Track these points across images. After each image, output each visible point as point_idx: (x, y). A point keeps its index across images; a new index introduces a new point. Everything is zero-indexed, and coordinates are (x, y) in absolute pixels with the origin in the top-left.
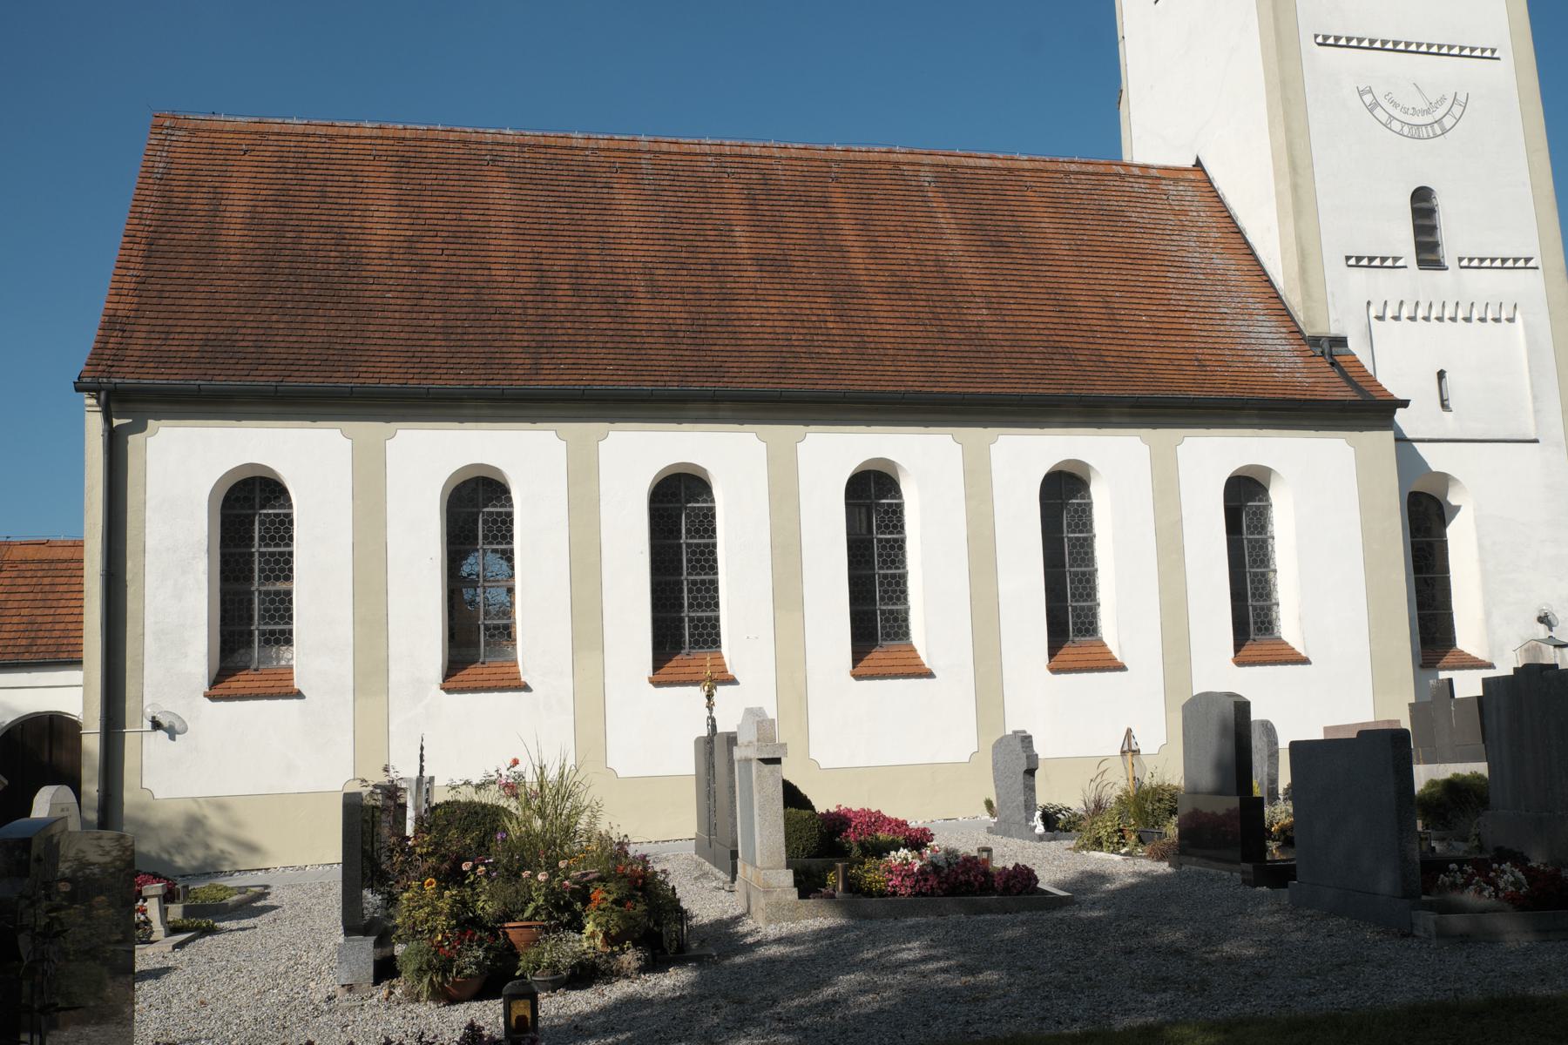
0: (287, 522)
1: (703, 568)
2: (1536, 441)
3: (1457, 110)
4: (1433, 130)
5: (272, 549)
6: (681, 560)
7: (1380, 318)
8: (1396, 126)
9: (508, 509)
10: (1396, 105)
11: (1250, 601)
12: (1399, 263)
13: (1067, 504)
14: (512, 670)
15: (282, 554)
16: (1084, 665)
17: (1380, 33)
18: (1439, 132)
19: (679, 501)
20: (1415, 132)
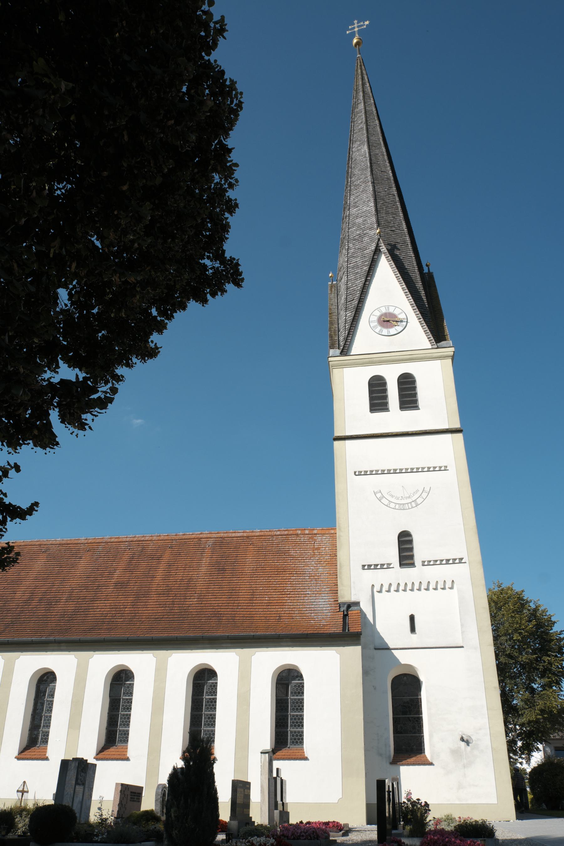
0: (301, 686)
1: (297, 709)
2: (462, 647)
3: (424, 495)
4: (408, 506)
5: (295, 697)
6: (203, 705)
7: (380, 592)
8: (392, 505)
9: (216, 681)
10: (392, 496)
11: (289, 728)
12: (391, 566)
13: (207, 683)
14: (301, 751)
15: (299, 699)
16: (118, 757)
17: (398, 467)
18: (410, 507)
20: (402, 507)
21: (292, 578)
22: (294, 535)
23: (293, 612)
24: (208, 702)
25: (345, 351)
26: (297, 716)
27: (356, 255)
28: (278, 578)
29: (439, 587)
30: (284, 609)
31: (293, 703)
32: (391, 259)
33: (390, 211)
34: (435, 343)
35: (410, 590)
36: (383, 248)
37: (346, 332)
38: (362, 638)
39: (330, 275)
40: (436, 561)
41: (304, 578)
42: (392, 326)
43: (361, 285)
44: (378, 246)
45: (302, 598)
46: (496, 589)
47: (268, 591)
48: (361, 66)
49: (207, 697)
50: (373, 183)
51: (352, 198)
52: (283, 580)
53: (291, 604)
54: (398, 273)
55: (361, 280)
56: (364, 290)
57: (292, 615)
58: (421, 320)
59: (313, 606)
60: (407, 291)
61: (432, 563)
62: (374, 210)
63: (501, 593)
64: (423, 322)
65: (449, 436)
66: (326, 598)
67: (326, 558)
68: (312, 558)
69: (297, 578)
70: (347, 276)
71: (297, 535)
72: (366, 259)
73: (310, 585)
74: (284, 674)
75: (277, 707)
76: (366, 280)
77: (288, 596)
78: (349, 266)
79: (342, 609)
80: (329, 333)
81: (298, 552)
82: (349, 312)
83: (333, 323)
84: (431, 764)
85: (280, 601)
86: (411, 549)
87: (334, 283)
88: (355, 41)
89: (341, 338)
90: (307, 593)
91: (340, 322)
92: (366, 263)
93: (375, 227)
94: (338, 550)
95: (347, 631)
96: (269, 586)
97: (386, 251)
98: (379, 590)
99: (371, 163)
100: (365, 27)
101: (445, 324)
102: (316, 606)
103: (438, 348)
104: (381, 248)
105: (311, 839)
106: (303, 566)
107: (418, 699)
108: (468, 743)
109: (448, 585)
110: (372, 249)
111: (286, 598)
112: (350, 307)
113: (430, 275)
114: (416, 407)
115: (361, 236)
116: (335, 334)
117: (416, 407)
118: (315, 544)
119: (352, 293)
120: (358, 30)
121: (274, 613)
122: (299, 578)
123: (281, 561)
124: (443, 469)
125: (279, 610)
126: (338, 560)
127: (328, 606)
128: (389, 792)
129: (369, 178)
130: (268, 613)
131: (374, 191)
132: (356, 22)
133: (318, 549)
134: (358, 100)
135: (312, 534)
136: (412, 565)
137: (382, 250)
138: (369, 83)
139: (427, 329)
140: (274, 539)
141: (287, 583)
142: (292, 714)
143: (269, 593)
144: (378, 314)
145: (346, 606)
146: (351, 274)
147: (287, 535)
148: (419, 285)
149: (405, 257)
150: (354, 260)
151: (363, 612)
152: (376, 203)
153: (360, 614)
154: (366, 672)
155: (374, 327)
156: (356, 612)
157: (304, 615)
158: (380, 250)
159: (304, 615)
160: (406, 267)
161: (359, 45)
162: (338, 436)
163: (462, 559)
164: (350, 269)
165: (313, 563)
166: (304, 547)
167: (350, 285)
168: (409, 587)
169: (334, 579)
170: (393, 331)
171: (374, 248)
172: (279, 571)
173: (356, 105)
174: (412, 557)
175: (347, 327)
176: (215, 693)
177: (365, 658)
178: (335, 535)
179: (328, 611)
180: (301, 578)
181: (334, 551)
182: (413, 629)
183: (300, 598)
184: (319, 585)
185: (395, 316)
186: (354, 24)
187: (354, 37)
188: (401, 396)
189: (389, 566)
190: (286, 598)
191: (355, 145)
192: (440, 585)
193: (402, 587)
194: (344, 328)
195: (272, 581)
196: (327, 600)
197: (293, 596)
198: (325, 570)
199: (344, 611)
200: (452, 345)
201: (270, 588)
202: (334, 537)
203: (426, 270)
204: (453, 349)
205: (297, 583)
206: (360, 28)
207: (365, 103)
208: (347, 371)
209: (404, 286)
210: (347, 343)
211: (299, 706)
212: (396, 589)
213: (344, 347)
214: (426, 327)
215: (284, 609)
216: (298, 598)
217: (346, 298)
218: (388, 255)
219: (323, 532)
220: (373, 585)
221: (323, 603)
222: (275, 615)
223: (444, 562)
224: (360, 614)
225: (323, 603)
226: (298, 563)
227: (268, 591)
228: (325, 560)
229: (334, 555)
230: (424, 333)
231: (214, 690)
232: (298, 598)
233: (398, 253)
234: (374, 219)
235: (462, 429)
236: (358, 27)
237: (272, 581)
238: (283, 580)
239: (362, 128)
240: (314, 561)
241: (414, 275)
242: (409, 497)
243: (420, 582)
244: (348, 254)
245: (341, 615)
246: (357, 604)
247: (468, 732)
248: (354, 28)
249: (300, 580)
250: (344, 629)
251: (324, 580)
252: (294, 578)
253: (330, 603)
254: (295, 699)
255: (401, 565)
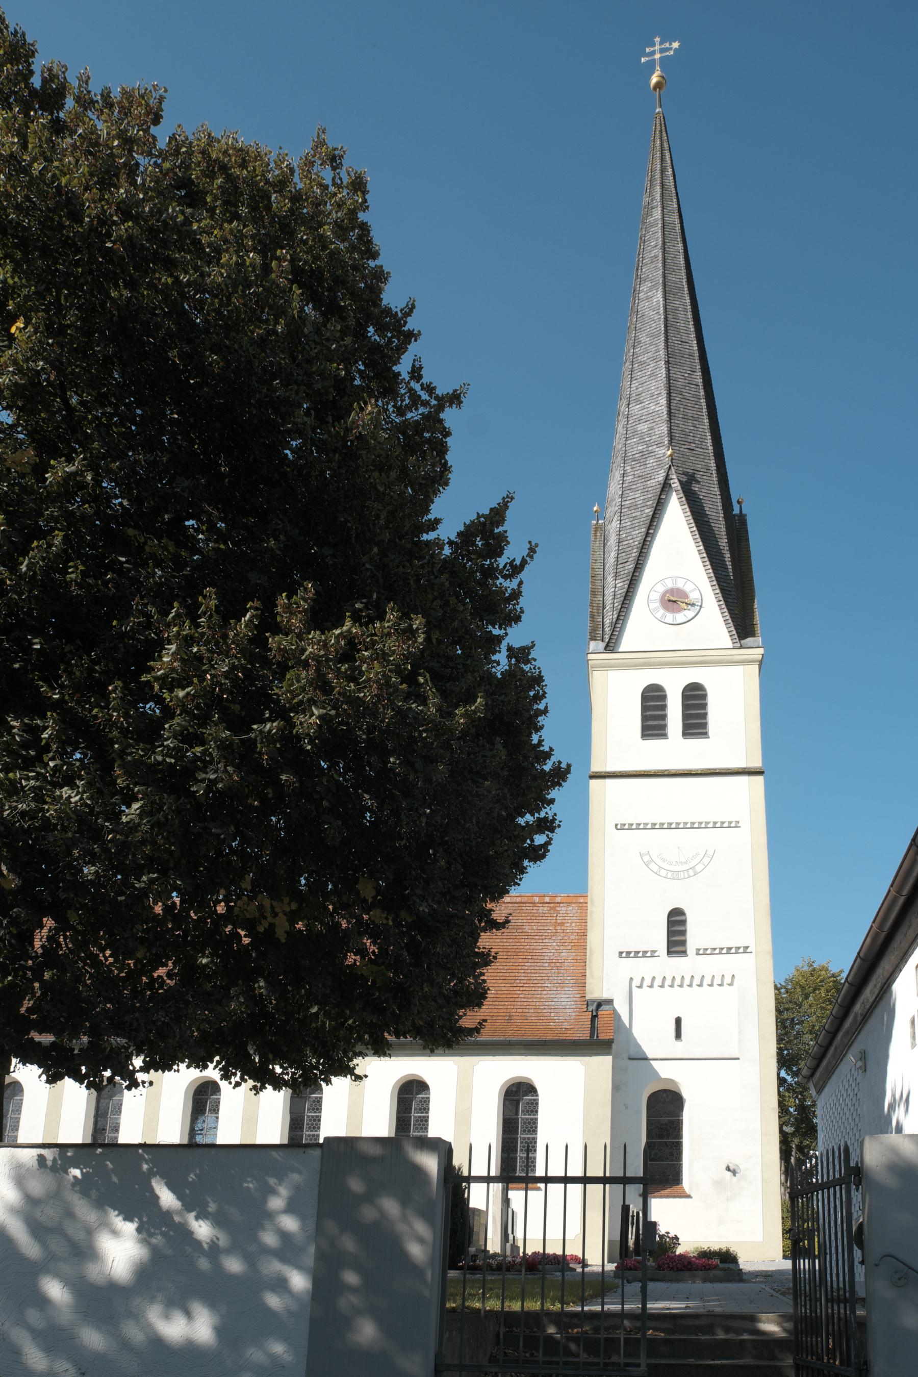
0: (535, 1103)
1: (529, 1131)
2: (738, 1059)
3: (706, 860)
5: (527, 1117)
6: (410, 1125)
7: (640, 987)
8: (663, 873)
9: (427, 1096)
10: (664, 860)
12: (656, 954)
15: (532, 1119)
17: (674, 820)
18: (686, 876)
19: (207, 1095)
20: (676, 876)
21: (526, 964)
22: (529, 903)
23: (527, 1011)
24: (417, 1121)
25: (611, 644)
26: (529, 1139)
27: (634, 487)
28: (508, 964)
29: (715, 983)
30: (516, 1007)
31: (525, 1123)
32: (685, 502)
33: (690, 413)
34: (737, 640)
35: (679, 986)
36: (675, 484)
37: (615, 613)
38: (614, 1046)
39: (595, 509)
40: (715, 949)
41: (542, 964)
42: (680, 610)
43: (640, 538)
44: (667, 478)
45: (539, 992)
46: (806, 968)
47: (494, 981)
48: (661, 131)
49: (416, 1115)
50: (667, 363)
51: (635, 384)
52: (515, 968)
53: (525, 1000)
54: (693, 525)
55: (640, 531)
56: (643, 551)
57: (526, 1014)
58: (722, 602)
59: (553, 1003)
60: (705, 555)
61: (709, 952)
62: (665, 413)
63: (812, 975)
64: (724, 606)
65: (745, 779)
66: (570, 992)
67: (572, 937)
68: (553, 938)
69: (533, 964)
70: (621, 520)
71: (534, 903)
72: (649, 496)
73: (549, 975)
74: (514, 1089)
75: (504, 1127)
76: (647, 534)
77: (521, 989)
78: (623, 503)
79: (590, 1008)
80: (590, 610)
81: (534, 927)
82: (619, 581)
83: (597, 592)
84: (689, 1197)
85: (511, 996)
86: (683, 933)
87: (600, 522)
88: (654, 79)
89: (607, 622)
90: (546, 985)
91: (606, 592)
92: (648, 503)
93: (666, 442)
94: (588, 928)
95: (595, 1038)
96: (495, 974)
97: (679, 488)
98: (639, 985)
99: (666, 326)
100: (672, 53)
101: (756, 606)
102: (557, 1003)
103: (741, 647)
104: (672, 481)
105: (552, 1264)
106: (540, 948)
107: (679, 1120)
108: (734, 1173)
109: (728, 980)
110: (660, 479)
111: (518, 992)
112: (622, 573)
113: (742, 518)
114: (705, 735)
115: (644, 455)
116: (598, 613)
117: (705, 735)
118: (558, 918)
119: (626, 550)
120: (661, 58)
121: (502, 1011)
122: (536, 964)
123: (511, 940)
124: (733, 825)
125: (509, 1007)
126: (588, 941)
127: (573, 1003)
128: (633, 1216)
129: (662, 353)
130: (496, 1011)
131: (669, 378)
132: (657, 39)
133: (562, 924)
134: (652, 200)
135: (554, 903)
136: (684, 953)
137: (673, 486)
138: (673, 167)
139: (728, 617)
140: (502, 908)
141: (520, 971)
142: (522, 1136)
143: (496, 985)
144: (661, 589)
145: (595, 1004)
146: (625, 517)
147: (521, 903)
148: (723, 543)
149: (706, 495)
150: (632, 495)
151: (617, 1012)
152: (670, 399)
153: (612, 1016)
154: (616, 1088)
155: (655, 609)
156: (608, 1012)
157: (541, 1014)
158: (670, 485)
159: (541, 1014)
160: (707, 513)
161: (660, 89)
162: (596, 773)
163: (747, 947)
164: (626, 510)
165: (555, 944)
166: (543, 921)
167: (624, 536)
168: (678, 982)
169: (581, 968)
170: (680, 617)
171: (662, 478)
172: (509, 954)
173: (649, 208)
174: (683, 943)
175: (616, 605)
176: (427, 1110)
177: (616, 1070)
178: (584, 905)
179: (572, 1010)
180: (539, 964)
181: (583, 927)
182: (678, 1035)
183: (536, 993)
184: (561, 975)
185: (686, 596)
186: (654, 45)
187: (654, 73)
188: (685, 717)
189: (653, 954)
190: (518, 992)
191: (644, 288)
192: (717, 981)
193: (668, 982)
194: (612, 606)
195: (499, 967)
196: (571, 996)
197: (527, 989)
198: (570, 954)
199: (592, 1011)
200: (761, 645)
201: (498, 978)
202: (583, 908)
203: (736, 511)
204: (761, 651)
205: (533, 971)
206: (664, 54)
207: (663, 208)
208: (614, 676)
209: (702, 548)
210: (614, 633)
211: (532, 1127)
212: (661, 984)
213: (610, 639)
214: (727, 614)
215: (516, 1007)
216: (533, 992)
217: (617, 557)
218: (682, 495)
219: (569, 900)
220: (631, 979)
221: (566, 1000)
222: (504, 1014)
223: (725, 951)
224: (612, 1016)
225: (566, 1000)
226: (535, 944)
227: (494, 981)
228: (570, 941)
229: (582, 934)
230: (723, 623)
231: (425, 1106)
232: (533, 992)
233: (696, 489)
234: (664, 429)
235: (764, 769)
236: (662, 51)
237: (499, 967)
238: (515, 968)
239: (656, 257)
240: (557, 941)
241: (717, 525)
242: (686, 863)
243: (692, 976)
244: (623, 484)
245: (588, 1016)
246: (610, 1002)
247: (733, 1162)
248: (653, 53)
249: (538, 968)
250: (592, 1035)
251: (568, 968)
252: (530, 964)
253: (575, 999)
254: (527, 1119)
255: (669, 953)
